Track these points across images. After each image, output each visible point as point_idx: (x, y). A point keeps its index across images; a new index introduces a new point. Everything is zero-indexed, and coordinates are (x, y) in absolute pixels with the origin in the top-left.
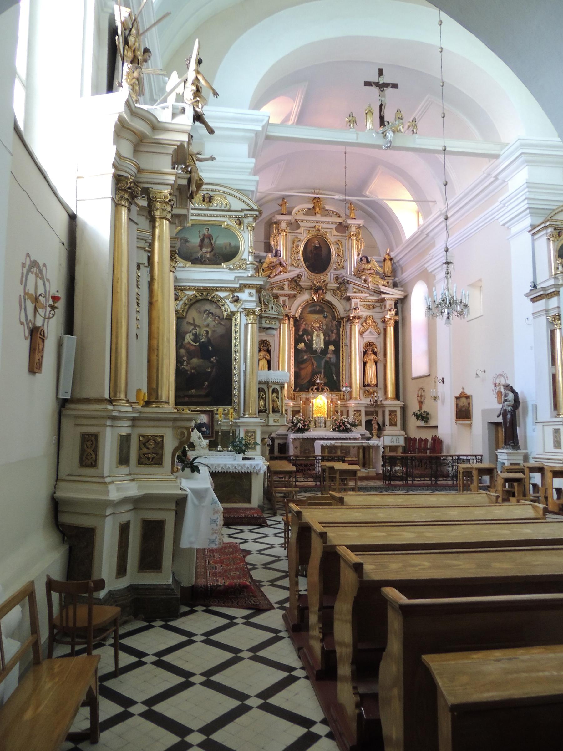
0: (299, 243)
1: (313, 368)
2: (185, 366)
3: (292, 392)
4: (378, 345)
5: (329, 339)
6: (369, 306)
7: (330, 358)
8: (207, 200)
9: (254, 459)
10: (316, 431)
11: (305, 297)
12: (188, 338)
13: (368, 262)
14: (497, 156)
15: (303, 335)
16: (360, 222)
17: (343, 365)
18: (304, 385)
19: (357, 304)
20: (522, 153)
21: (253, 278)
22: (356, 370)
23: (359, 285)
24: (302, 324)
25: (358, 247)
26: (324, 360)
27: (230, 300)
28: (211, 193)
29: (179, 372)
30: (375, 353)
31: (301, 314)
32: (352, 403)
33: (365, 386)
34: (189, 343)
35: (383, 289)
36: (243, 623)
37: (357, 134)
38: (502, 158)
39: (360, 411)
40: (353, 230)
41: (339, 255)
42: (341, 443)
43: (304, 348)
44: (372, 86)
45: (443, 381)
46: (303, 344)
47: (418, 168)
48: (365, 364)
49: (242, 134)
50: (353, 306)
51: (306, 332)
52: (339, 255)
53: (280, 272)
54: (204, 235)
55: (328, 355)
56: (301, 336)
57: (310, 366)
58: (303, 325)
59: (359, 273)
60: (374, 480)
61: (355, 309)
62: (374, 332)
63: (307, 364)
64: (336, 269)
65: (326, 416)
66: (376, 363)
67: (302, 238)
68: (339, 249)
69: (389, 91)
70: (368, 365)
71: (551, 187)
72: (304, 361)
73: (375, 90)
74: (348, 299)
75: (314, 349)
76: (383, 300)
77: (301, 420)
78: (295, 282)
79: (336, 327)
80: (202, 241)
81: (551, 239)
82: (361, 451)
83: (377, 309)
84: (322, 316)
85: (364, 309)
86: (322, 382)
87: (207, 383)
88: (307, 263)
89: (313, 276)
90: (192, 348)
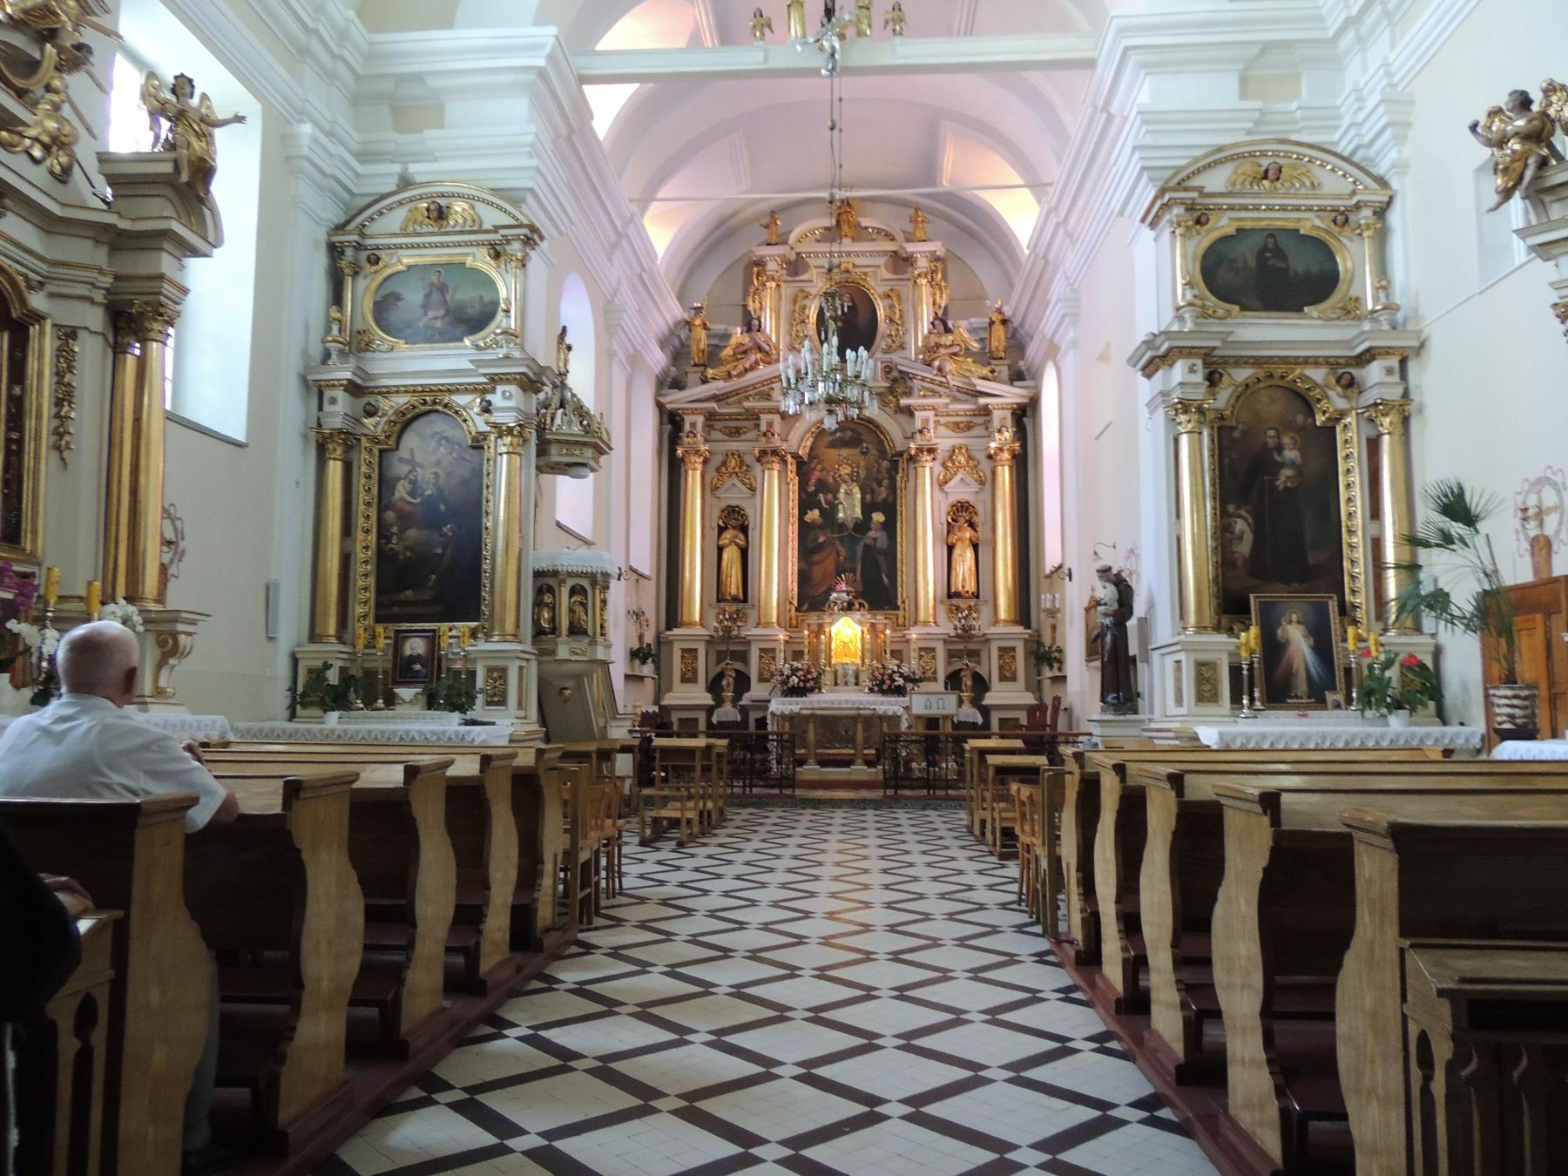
0: (806, 302)
3: (793, 612)
4: (980, 508)
6: (957, 424)
7: (875, 539)
8: (434, 215)
12: (401, 490)
13: (948, 330)
14: (1090, 64)
15: (816, 493)
16: (936, 247)
17: (902, 549)
18: (812, 597)
19: (926, 421)
20: (1126, 49)
21: (508, 362)
22: (925, 562)
23: (932, 381)
27: (477, 410)
28: (442, 202)
29: (384, 558)
30: (972, 525)
31: (812, 449)
32: (913, 633)
33: (950, 596)
34: (402, 499)
35: (982, 386)
36: (905, 1118)
37: (767, 52)
38: (1100, 63)
39: (933, 650)
40: (923, 264)
41: (891, 320)
46: (816, 512)
47: (1012, 115)
48: (950, 549)
49: (510, 77)
50: (918, 425)
51: (822, 486)
52: (891, 320)
53: (757, 363)
54: (432, 284)
55: (871, 534)
56: (813, 493)
57: (832, 557)
59: (930, 352)
61: (921, 432)
62: (969, 479)
63: (824, 554)
64: (888, 351)
65: (859, 661)
66: (975, 547)
67: (813, 291)
68: (892, 307)
70: (957, 551)
72: (820, 547)
74: (909, 412)
76: (986, 412)
77: (798, 669)
80: (428, 296)
81: (1178, 232)
83: (977, 431)
84: (857, 451)
85: (949, 433)
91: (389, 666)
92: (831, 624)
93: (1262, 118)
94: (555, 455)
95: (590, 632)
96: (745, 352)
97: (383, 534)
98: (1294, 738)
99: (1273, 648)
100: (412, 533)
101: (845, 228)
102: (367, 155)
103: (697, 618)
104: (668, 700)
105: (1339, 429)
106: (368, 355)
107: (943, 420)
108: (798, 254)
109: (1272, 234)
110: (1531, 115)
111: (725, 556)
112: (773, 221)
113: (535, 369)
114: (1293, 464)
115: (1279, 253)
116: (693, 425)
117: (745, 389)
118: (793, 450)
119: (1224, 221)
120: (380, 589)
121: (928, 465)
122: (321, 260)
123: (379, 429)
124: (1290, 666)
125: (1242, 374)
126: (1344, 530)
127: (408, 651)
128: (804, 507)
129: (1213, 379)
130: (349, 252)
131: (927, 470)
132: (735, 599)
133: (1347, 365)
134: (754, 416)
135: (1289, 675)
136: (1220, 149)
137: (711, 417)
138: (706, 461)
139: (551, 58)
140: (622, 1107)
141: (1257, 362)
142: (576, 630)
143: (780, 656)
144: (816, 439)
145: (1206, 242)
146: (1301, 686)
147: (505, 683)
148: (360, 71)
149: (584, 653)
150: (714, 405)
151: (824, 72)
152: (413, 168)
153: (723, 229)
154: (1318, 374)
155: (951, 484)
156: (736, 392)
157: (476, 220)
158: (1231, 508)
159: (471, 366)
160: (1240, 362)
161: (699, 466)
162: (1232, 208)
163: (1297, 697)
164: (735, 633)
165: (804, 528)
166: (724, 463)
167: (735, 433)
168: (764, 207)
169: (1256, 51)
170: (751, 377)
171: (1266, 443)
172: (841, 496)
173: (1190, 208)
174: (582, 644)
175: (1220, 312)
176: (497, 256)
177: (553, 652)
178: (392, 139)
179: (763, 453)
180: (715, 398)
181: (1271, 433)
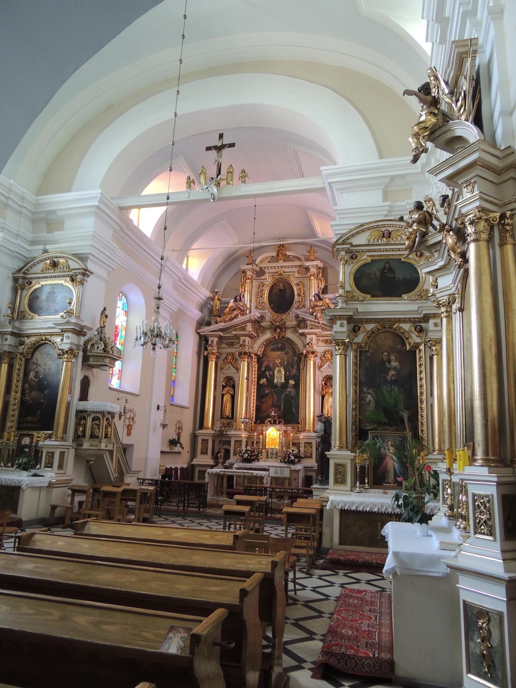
1: (273, 402)
2: (27, 398)
5: (290, 374)
7: (290, 392)
9: (43, 476)
10: (268, 461)
11: (268, 335)
12: (32, 375)
15: (265, 371)
17: (301, 397)
18: (261, 418)
19: (311, 339)
24: (265, 360)
25: (318, 285)
26: (284, 394)
28: (55, 260)
29: (23, 403)
32: (302, 436)
34: (32, 379)
39: (311, 443)
41: (299, 295)
42: (225, 471)
43: (266, 383)
44: (212, 150)
45: (158, 408)
46: (265, 379)
48: (323, 397)
49: (86, 210)
50: (308, 341)
51: (268, 368)
52: (299, 295)
55: (289, 390)
56: (264, 372)
58: (266, 362)
60: (216, 508)
61: (308, 344)
67: (267, 283)
68: (300, 289)
69: (226, 151)
70: (326, 398)
71: (360, 210)
72: (266, 395)
73: (214, 152)
75: (275, 383)
78: (257, 323)
79: (297, 362)
82: (225, 480)
85: (324, 344)
86: (276, 414)
87: (39, 412)
88: (272, 305)
89: (276, 316)
90: (33, 383)
91: (15, 448)
92: (266, 430)
93: (391, 209)
94: (91, 362)
95: (100, 437)
96: (234, 310)
97: (23, 394)
98: (368, 505)
99: (379, 460)
100: (34, 393)
101: (280, 256)
102: (34, 243)
103: (210, 426)
104: (194, 462)
105: (417, 352)
106: (24, 320)
107: (321, 339)
108: (261, 268)
109: (388, 261)
110: (421, 212)
111: (225, 398)
112: (250, 255)
113: (80, 327)
114: (395, 369)
115: (391, 270)
116: (212, 342)
117: (235, 326)
118: (256, 352)
119: (365, 257)
120: (20, 416)
121: (312, 359)
122: (10, 284)
123: (24, 351)
124: (386, 467)
125: (370, 327)
126: (419, 400)
127: (23, 443)
128: (259, 378)
129: (355, 330)
130: (20, 281)
131: (312, 361)
132: (228, 418)
133: (420, 322)
134: (237, 337)
135: (385, 472)
136: (362, 225)
137: (220, 338)
138: (217, 358)
139: (101, 201)
140: (292, 645)
141: (376, 321)
142: (93, 436)
143: (244, 444)
144: (266, 347)
145: (356, 267)
146: (391, 477)
147: (53, 458)
148: (33, 211)
149: (96, 446)
150: (221, 333)
151: (212, 200)
152: (48, 247)
153: (231, 259)
154: (406, 327)
155: (324, 367)
156: (231, 327)
157: (68, 267)
158: (365, 390)
159: (54, 326)
160: (369, 321)
161: (214, 360)
162: (368, 251)
163: (388, 483)
164: (224, 433)
165: (260, 387)
166: (226, 358)
167: (231, 345)
168: (248, 249)
169: (388, 180)
170: (235, 321)
171: (383, 359)
172: (276, 372)
173: (348, 251)
174: (95, 442)
175: (361, 298)
176: (73, 280)
177: (82, 445)
178: (44, 235)
179: (240, 354)
180: (222, 330)
181: (385, 354)
